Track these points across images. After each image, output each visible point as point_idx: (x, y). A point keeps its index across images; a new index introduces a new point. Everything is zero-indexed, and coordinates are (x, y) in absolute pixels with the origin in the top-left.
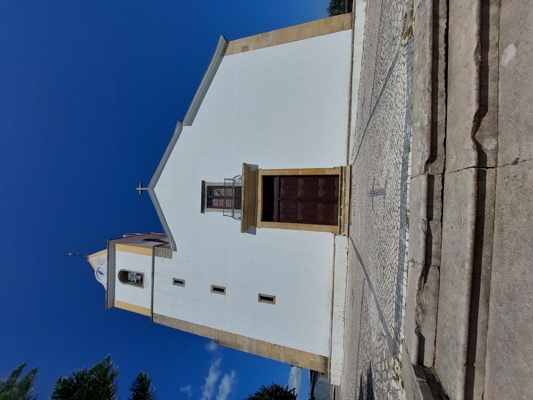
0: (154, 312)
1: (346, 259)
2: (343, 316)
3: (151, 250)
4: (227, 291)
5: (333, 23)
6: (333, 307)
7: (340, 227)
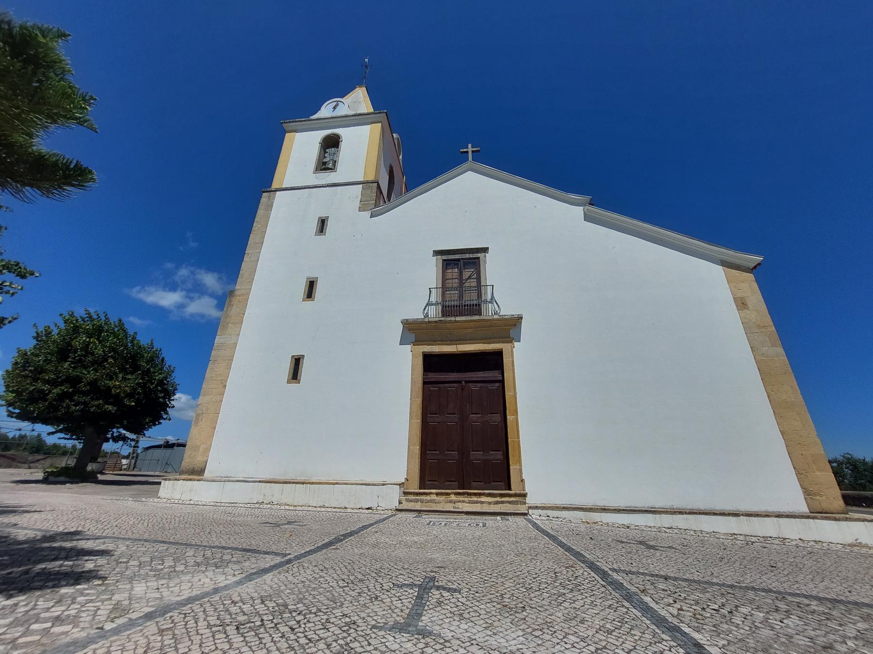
3: (371, 177)
5: (818, 473)
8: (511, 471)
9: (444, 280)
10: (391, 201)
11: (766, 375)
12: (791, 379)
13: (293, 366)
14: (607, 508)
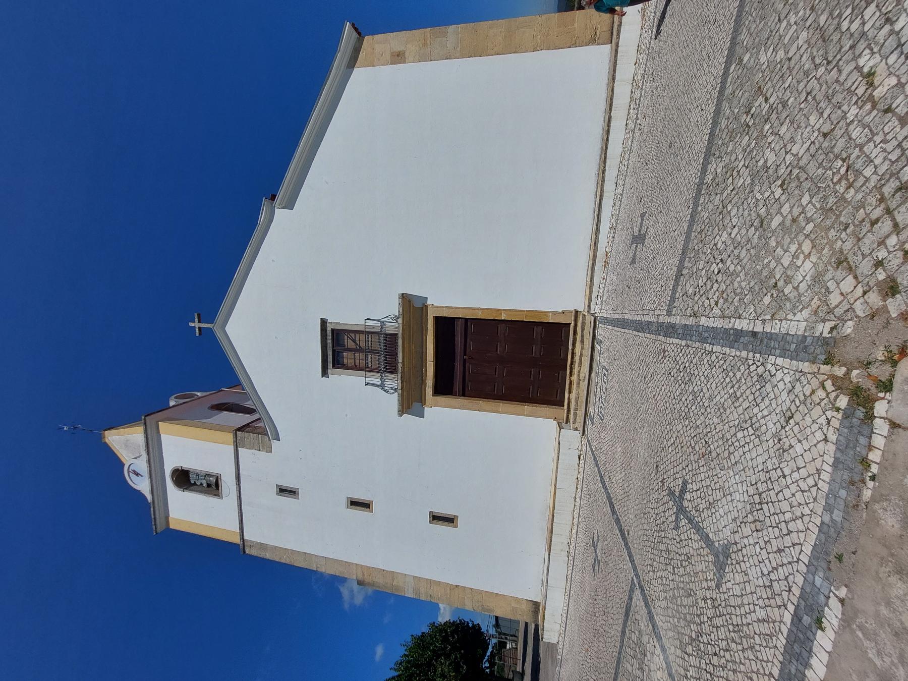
0: (245, 538)
1: (577, 466)
2: (567, 550)
3: (230, 437)
4: (374, 506)
5: (576, 25)
6: (551, 537)
7: (569, 410)
8: (554, 322)
9: (355, 368)
10: (254, 408)
11: (476, 51)
12: (483, 26)
13: (441, 522)
14: (593, 243)
